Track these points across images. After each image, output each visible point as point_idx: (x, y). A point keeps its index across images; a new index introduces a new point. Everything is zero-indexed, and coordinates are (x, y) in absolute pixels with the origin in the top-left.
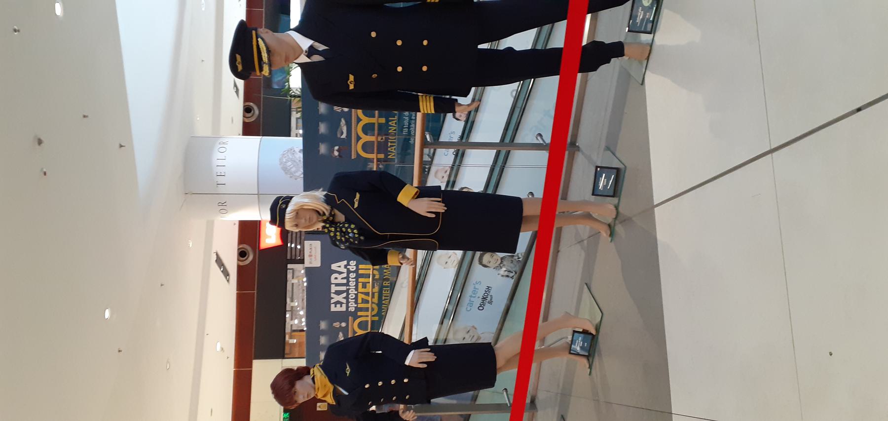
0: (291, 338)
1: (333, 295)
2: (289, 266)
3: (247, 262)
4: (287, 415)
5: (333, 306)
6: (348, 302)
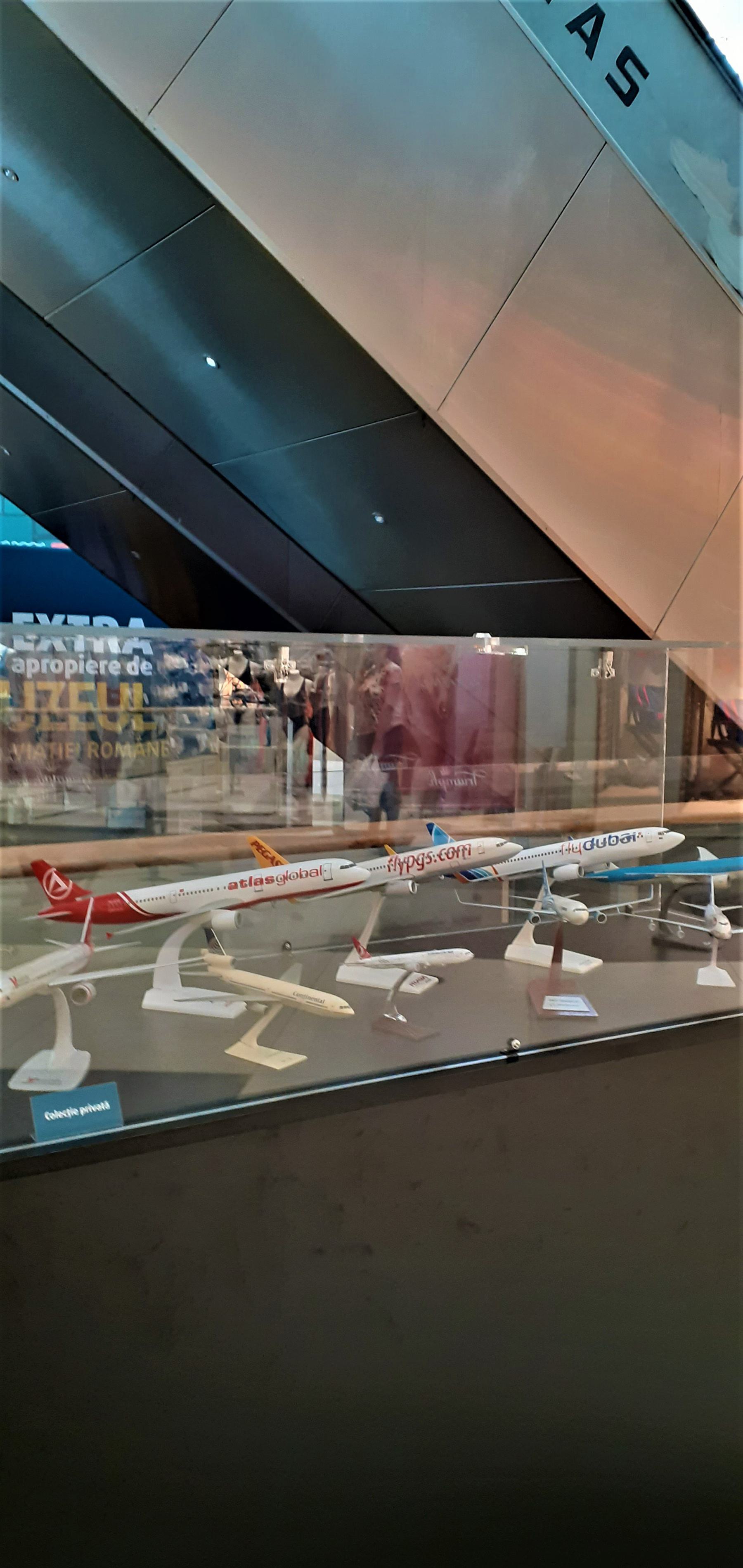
6: (39, 656)
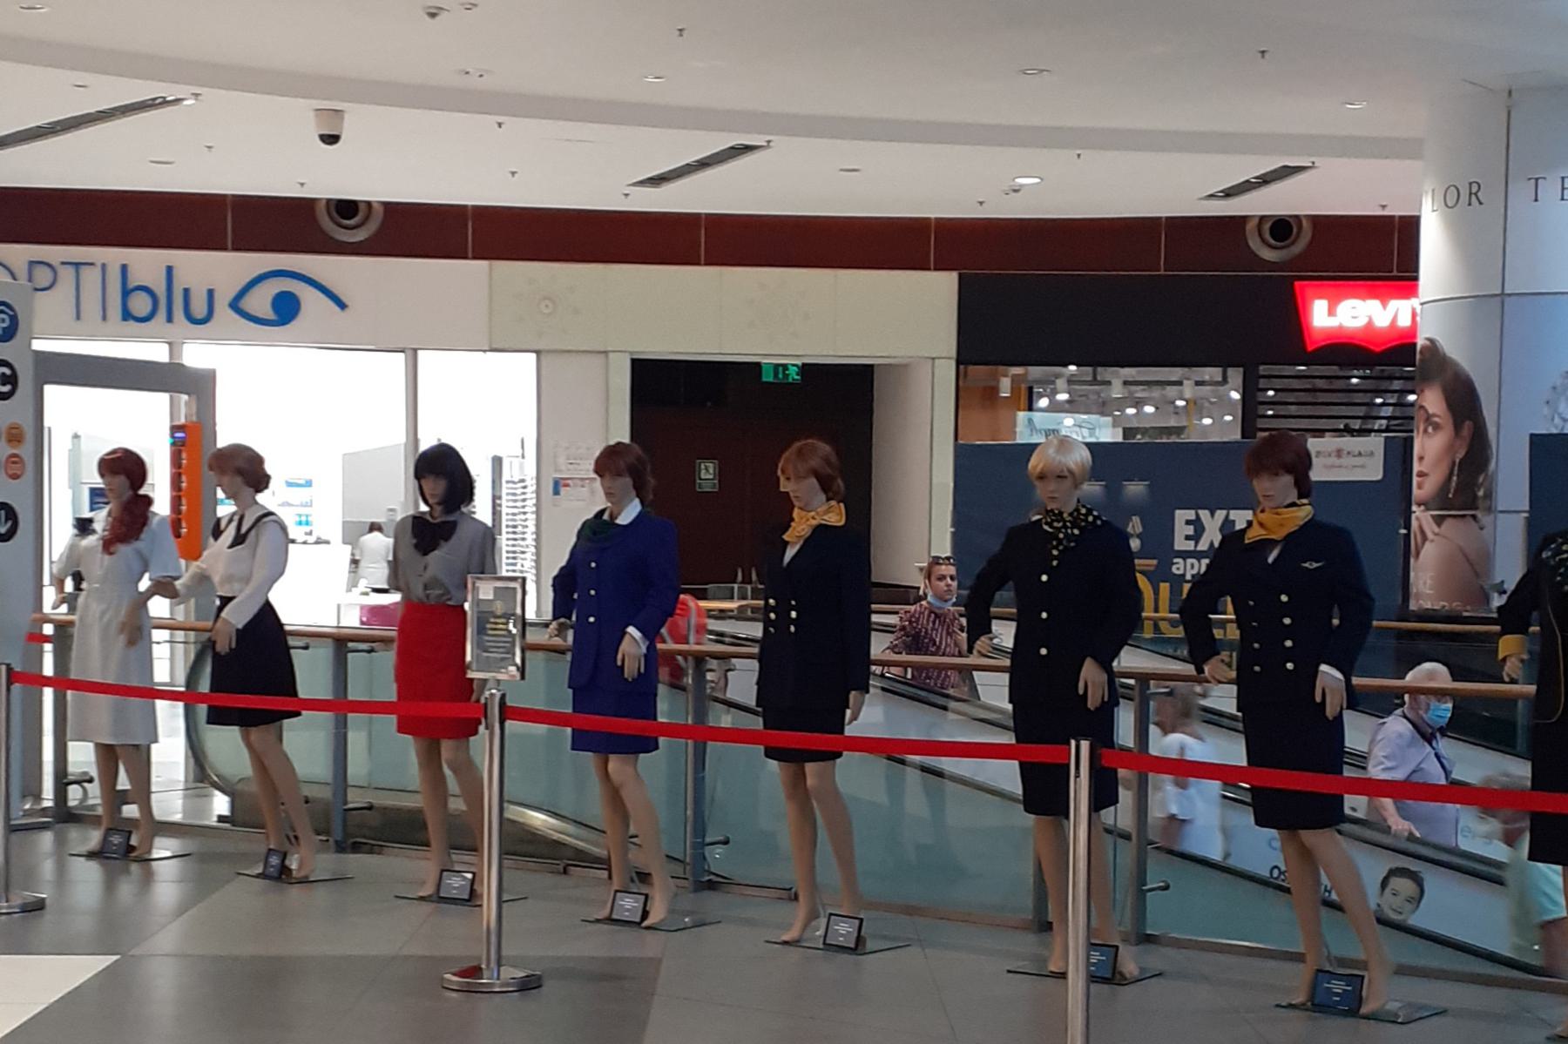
0: (1015, 379)
1: (1221, 515)
2: (1236, 375)
3: (1254, 243)
4: (793, 374)
5: (1191, 515)
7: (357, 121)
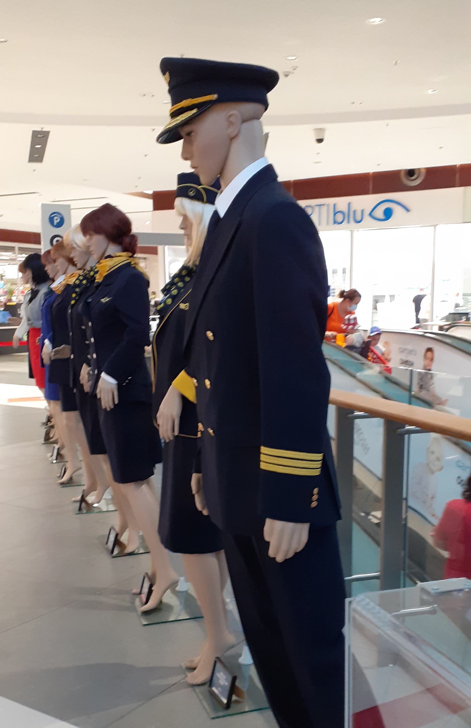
7: (332, 131)
